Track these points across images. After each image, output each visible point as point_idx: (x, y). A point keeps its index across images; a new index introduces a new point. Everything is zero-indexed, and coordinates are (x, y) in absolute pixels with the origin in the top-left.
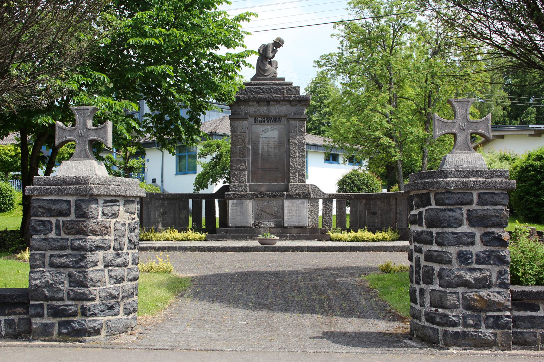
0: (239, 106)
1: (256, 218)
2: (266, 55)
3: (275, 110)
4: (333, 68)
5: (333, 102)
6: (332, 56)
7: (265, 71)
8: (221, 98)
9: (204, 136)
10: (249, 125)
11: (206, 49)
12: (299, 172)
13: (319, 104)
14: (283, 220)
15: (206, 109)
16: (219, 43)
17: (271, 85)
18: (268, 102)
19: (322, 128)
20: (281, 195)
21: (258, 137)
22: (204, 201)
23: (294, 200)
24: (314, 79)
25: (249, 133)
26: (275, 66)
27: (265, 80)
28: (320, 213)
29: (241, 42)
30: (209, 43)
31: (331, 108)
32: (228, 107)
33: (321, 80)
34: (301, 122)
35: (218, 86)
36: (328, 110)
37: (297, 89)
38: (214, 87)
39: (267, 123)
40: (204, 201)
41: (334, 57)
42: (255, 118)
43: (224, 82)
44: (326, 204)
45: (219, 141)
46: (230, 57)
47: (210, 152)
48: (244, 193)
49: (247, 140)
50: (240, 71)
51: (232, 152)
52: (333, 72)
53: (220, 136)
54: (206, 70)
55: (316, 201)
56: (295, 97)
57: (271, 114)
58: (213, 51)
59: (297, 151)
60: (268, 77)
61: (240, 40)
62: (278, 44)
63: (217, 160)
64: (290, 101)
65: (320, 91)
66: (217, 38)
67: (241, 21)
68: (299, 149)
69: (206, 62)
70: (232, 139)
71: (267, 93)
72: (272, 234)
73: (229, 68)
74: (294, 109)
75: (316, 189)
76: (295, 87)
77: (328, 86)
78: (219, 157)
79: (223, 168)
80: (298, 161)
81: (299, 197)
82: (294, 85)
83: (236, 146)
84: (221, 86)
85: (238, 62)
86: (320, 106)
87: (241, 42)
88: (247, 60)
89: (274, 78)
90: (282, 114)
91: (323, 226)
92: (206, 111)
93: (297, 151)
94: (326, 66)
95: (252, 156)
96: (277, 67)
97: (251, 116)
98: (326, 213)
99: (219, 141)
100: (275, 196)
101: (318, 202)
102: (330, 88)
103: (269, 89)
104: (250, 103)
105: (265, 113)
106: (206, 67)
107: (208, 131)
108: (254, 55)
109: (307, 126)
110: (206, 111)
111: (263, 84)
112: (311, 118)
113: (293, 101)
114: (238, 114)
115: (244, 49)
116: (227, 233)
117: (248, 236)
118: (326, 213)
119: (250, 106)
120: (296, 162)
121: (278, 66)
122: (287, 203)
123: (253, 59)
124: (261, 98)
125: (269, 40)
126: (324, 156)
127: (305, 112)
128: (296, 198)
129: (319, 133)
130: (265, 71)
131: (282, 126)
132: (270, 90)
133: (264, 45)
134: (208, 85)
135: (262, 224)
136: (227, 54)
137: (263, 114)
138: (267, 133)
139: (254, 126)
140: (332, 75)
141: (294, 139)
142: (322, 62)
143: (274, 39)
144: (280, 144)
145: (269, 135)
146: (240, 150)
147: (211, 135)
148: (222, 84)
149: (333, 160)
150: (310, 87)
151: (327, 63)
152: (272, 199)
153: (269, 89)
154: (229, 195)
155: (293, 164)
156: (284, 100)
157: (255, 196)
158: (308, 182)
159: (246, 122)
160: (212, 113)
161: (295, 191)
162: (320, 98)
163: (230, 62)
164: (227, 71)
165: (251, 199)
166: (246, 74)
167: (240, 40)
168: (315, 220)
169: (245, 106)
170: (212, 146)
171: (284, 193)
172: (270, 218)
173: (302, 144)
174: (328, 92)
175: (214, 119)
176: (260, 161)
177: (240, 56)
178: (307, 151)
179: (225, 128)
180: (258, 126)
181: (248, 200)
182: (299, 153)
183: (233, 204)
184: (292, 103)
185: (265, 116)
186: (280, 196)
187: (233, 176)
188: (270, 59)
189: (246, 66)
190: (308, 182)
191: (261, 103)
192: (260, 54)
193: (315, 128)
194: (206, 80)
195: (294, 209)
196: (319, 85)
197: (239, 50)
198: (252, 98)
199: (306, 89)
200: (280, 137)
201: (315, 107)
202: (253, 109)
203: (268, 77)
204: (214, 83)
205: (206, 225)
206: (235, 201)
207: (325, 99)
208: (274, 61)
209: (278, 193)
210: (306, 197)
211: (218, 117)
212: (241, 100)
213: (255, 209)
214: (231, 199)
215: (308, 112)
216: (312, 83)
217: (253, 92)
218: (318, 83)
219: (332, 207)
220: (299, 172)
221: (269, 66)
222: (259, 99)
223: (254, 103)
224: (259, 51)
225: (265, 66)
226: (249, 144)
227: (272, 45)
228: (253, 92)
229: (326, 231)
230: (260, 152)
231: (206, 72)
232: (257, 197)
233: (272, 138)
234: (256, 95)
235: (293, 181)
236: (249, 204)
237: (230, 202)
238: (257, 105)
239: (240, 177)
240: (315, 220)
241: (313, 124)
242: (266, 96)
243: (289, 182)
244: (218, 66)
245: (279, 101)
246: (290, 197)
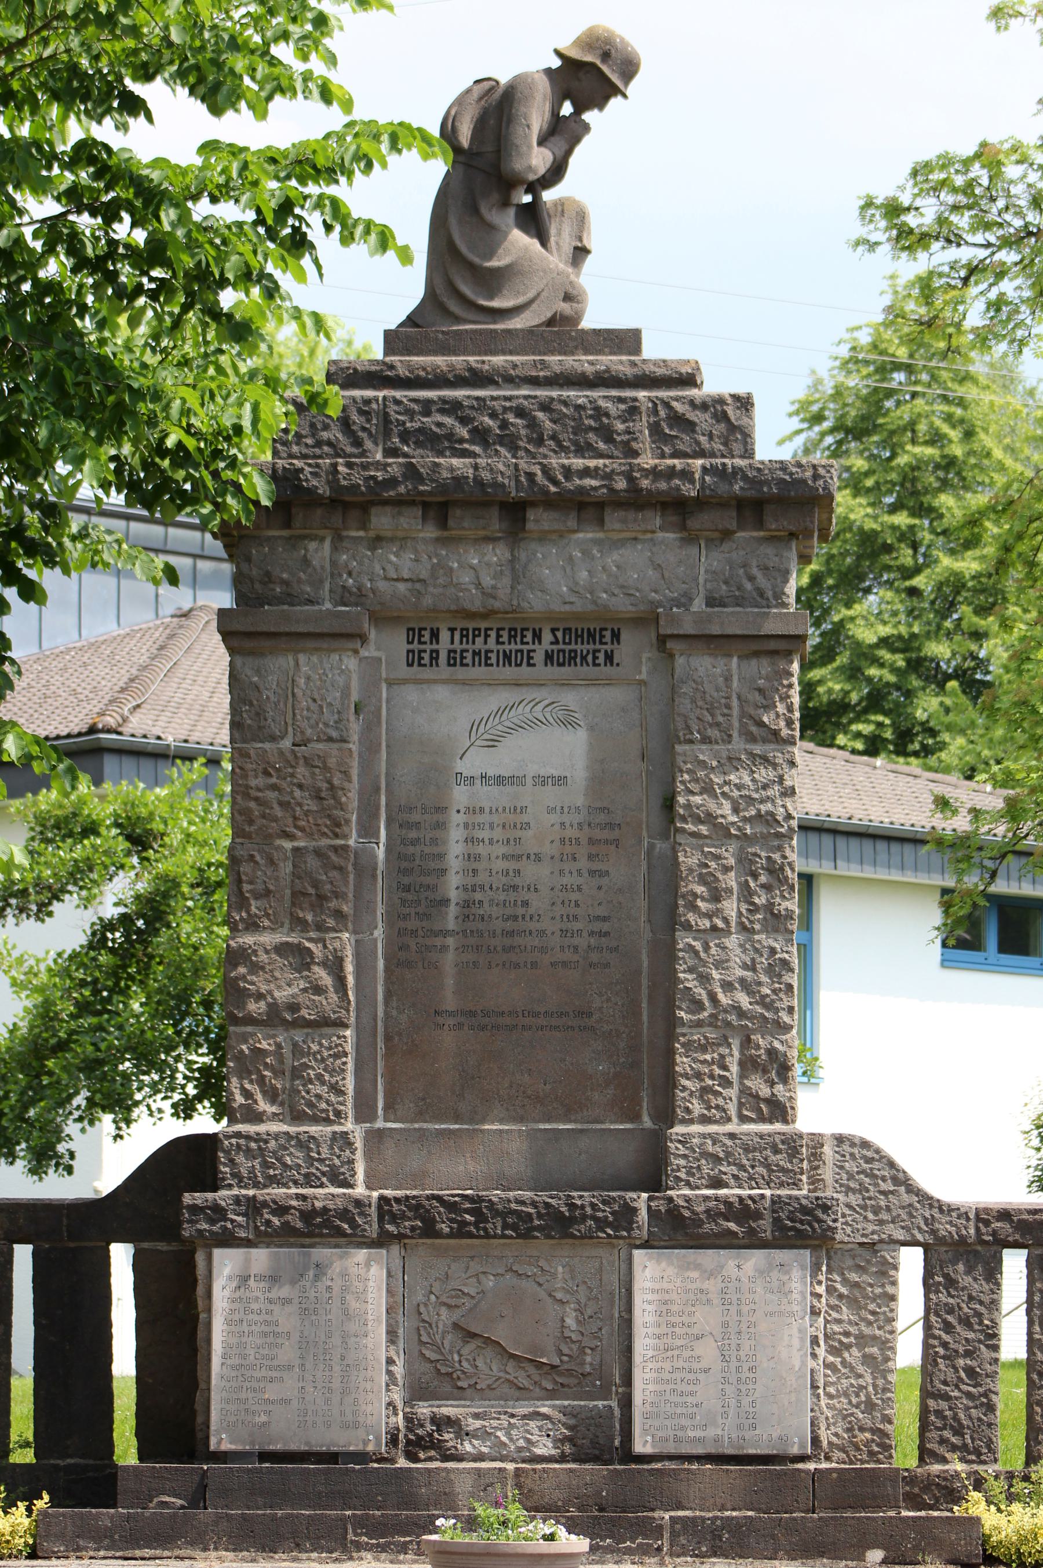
0: (293, 542)
1: (417, 1392)
2: (498, 163)
3: (570, 569)
4: (1009, 256)
5: (1002, 508)
6: (995, 167)
7: (493, 280)
8: (166, 483)
9: (28, 758)
10: (370, 686)
11: (55, 111)
12: (747, 1042)
13: (902, 519)
14: (627, 1403)
15: (51, 558)
16: (146, 74)
17: (534, 382)
18: (513, 512)
19: (927, 706)
20: (606, 1212)
21: (436, 774)
22: (23, 1255)
23: (708, 1257)
24: (865, 338)
25: (370, 748)
26: (567, 247)
27: (490, 343)
28: (909, 1350)
29: (316, 65)
30: (73, 68)
31: (990, 550)
32: (217, 547)
33: (913, 342)
34: (765, 666)
35: (138, 395)
36: (969, 565)
37: (732, 416)
38: (105, 402)
39: (509, 672)
40: (23, 1255)
41: (1012, 171)
42: (414, 634)
43: (185, 362)
44: (951, 1283)
45: (153, 797)
46: (229, 170)
47: (81, 876)
48: (326, 1194)
49: (352, 798)
50: (301, 276)
51: (239, 885)
52: (1007, 287)
53: (153, 756)
54: (51, 269)
55: (877, 1260)
56: (721, 473)
57: (535, 602)
58: (105, 132)
59: (731, 880)
60: (517, 323)
61: (304, 49)
62: (590, 77)
63: (129, 946)
64: (678, 509)
65: (911, 426)
66: (134, 31)
67: (343, 180)
68: (747, 865)
69: (51, 208)
70: (241, 791)
71: (512, 445)
72: (538, 1507)
73: (221, 258)
74: (706, 565)
75: (872, 1168)
76: (720, 401)
77: (970, 392)
78: (154, 909)
79: (174, 1004)
80: (737, 957)
81: (742, 1228)
82: (715, 384)
83: (268, 838)
84: (157, 396)
85: (286, 208)
86: (909, 538)
87: (316, 65)
88: (358, 195)
89: (562, 329)
90: (621, 605)
91: (925, 1454)
92: (48, 578)
93: (731, 880)
94: (954, 240)
95: (390, 920)
96: (581, 253)
97: (382, 618)
98: (951, 1357)
99: (153, 797)
100: (561, 1225)
101: (887, 1271)
102: (982, 399)
103: (520, 412)
104: (382, 520)
105: (489, 595)
106: (50, 249)
107: (67, 721)
108: (411, 157)
109: (808, 689)
110: (48, 578)
111: (476, 378)
112: (840, 625)
113: (701, 503)
114: (290, 598)
115: (333, 119)
116: (198, 1498)
117: (360, 1524)
118: (951, 1357)
119: (377, 541)
120: (720, 964)
121: (593, 241)
122: (652, 1273)
123: (405, 192)
124: (459, 481)
125: (526, 55)
126: (936, 917)
127: (791, 589)
128: (725, 1241)
129: (908, 741)
130: (493, 280)
131: (617, 695)
132: (533, 424)
133: (486, 86)
134: (59, 383)
135: (462, 1434)
136: (209, 147)
137: (476, 605)
138: (508, 742)
139: (411, 694)
140: (997, 305)
141: (708, 789)
142: (926, 214)
143: (566, 38)
144: (602, 832)
145: (516, 759)
146: (296, 875)
147: (88, 751)
148: (168, 378)
149: (1005, 947)
150: (838, 393)
151: (962, 221)
152: (541, 1245)
153: (520, 412)
154: (218, 1212)
155: (704, 979)
156: (635, 500)
157: (409, 1225)
158: (814, 1113)
159: (351, 663)
160: (97, 584)
161: (717, 1183)
162: (909, 478)
163: (228, 212)
164: (204, 282)
165: (382, 1241)
166: (354, 297)
167: (304, 49)
168: (870, 1406)
169: (338, 539)
170: (91, 829)
171: (628, 1198)
172: (522, 1392)
173: (770, 829)
174: (969, 435)
175: (111, 628)
176: (450, 958)
177: (306, 165)
178: (808, 879)
179: (192, 698)
180: (441, 693)
181: (361, 1254)
182: (746, 894)
183: (243, 1280)
184: (693, 523)
185: (486, 615)
186: (602, 1224)
187: (244, 1072)
188: (533, 188)
189: (347, 239)
190: (814, 1113)
191: (463, 522)
192: (457, 150)
193: (875, 701)
194: (47, 344)
195: (707, 1319)
196: (900, 377)
197: (292, 123)
198: (392, 482)
199: (804, 405)
200: (600, 778)
201: (872, 547)
202: (400, 562)
203: (517, 323)
204: (104, 365)
205: (42, 1441)
206: (260, 1257)
207: (945, 485)
208: (561, 205)
209: (583, 1198)
210: (800, 1229)
211: (137, 616)
212: (309, 499)
213: (407, 1318)
214: (228, 1240)
215: (817, 580)
216: (852, 362)
217: (405, 436)
218: (897, 367)
219: (994, 1305)
220: (747, 1042)
221: (519, 241)
222: (443, 488)
223: (410, 521)
224: (449, 131)
225: (490, 237)
226: (368, 831)
227: (544, 86)
228: (405, 436)
229: (950, 1493)
230: (453, 885)
231: (52, 287)
232: (429, 1230)
233: (542, 781)
234: (423, 459)
235: (697, 1108)
236: (366, 1279)
237: (226, 1271)
238: (431, 532)
239: (296, 1073)
240: (870, 1406)
241: (853, 673)
242: (498, 465)
243: (666, 1115)
244: (140, 236)
245: (600, 506)
246: (679, 1231)
